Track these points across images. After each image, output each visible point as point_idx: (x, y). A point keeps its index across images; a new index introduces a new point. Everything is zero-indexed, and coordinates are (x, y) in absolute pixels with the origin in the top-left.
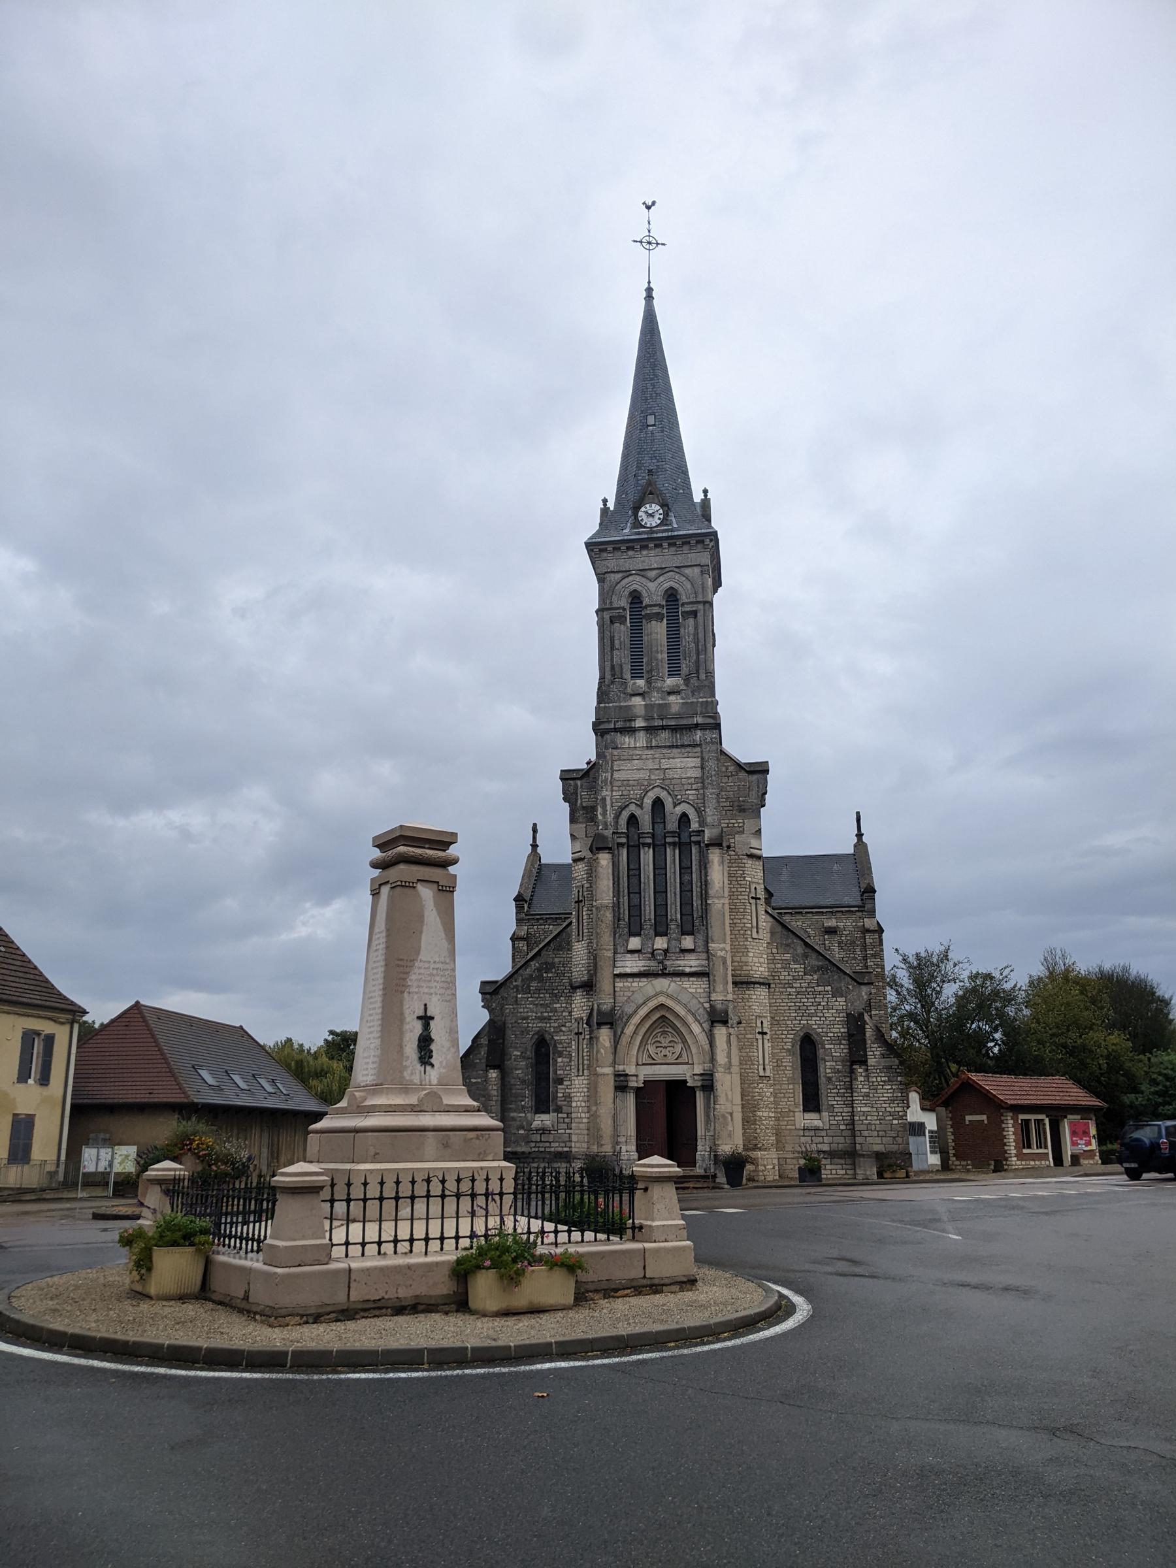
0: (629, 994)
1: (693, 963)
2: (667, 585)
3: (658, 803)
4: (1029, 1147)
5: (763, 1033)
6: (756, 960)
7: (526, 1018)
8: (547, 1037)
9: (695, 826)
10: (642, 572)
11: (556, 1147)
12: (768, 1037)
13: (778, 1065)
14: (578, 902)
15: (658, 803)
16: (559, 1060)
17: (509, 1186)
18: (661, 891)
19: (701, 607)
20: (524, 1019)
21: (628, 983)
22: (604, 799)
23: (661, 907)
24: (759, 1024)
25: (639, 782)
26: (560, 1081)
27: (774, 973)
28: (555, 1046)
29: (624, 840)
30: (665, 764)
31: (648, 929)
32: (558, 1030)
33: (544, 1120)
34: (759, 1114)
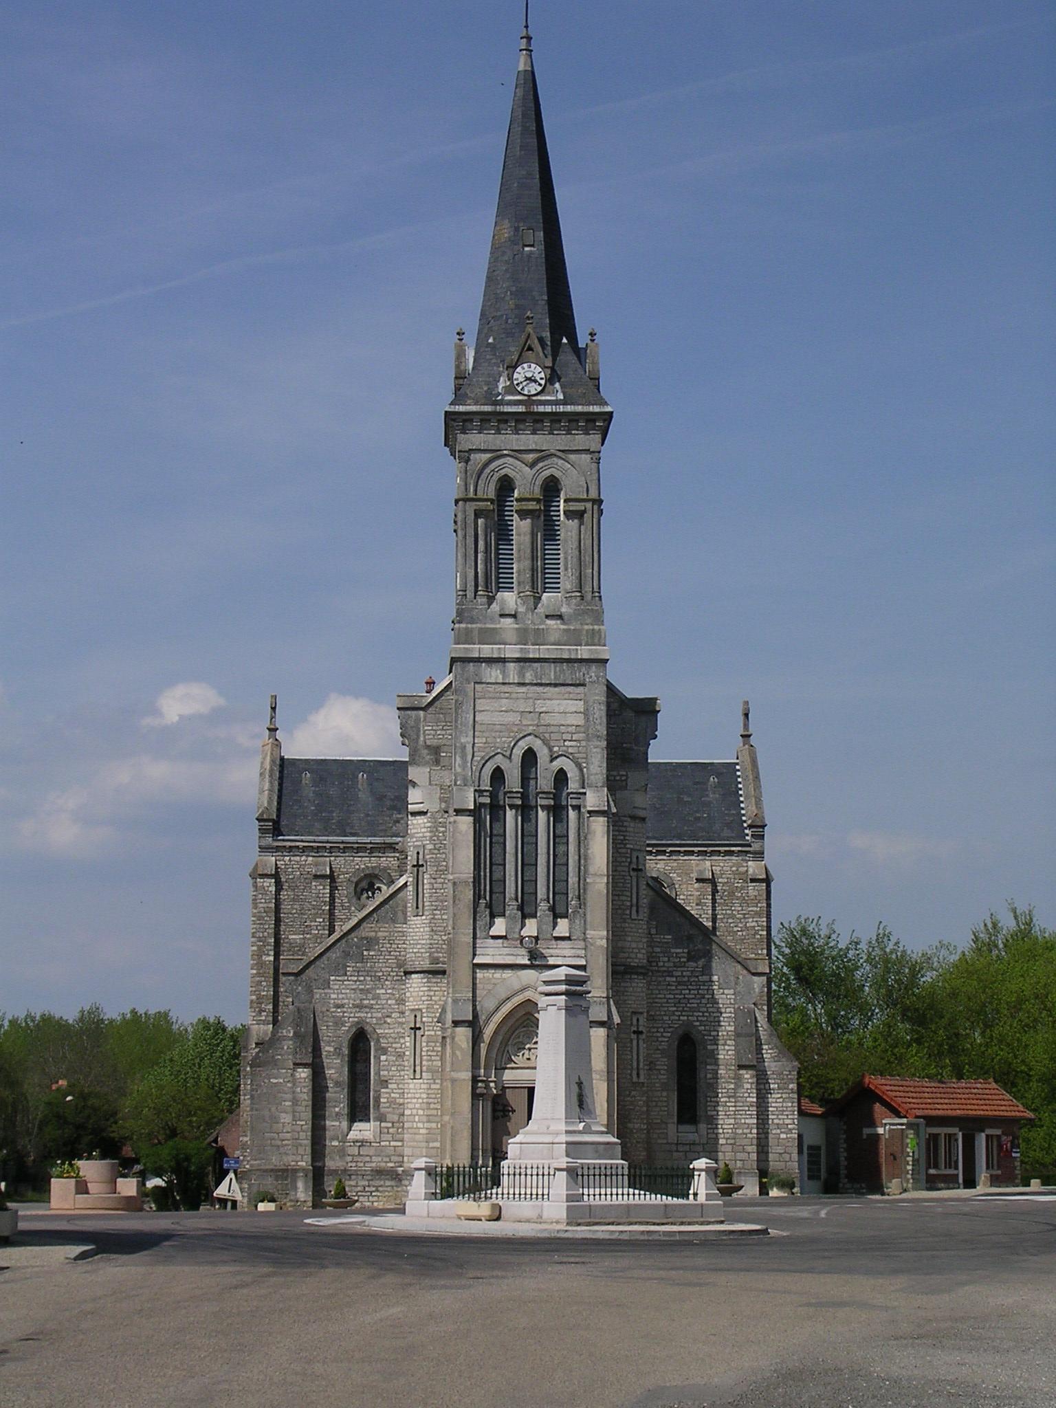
0: (490, 987)
1: (567, 952)
2: (547, 473)
3: (530, 757)
4: (936, 1166)
5: (638, 1033)
6: (634, 945)
7: (342, 1006)
8: (367, 1028)
9: (573, 786)
10: (517, 453)
11: (377, 1162)
12: (644, 1036)
13: (651, 1065)
14: (418, 866)
15: (530, 757)
16: (383, 1058)
17: (626, 1172)
18: (528, 864)
19: (589, 505)
20: (338, 1006)
21: (489, 974)
22: (464, 748)
23: (528, 884)
24: (635, 1022)
25: (507, 727)
26: (384, 1083)
27: (652, 958)
28: (378, 1041)
29: (488, 800)
30: (541, 706)
31: (512, 908)
32: (382, 1021)
33: (363, 1130)
34: (630, 1125)
